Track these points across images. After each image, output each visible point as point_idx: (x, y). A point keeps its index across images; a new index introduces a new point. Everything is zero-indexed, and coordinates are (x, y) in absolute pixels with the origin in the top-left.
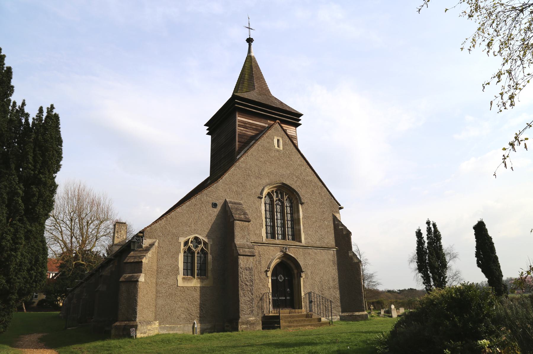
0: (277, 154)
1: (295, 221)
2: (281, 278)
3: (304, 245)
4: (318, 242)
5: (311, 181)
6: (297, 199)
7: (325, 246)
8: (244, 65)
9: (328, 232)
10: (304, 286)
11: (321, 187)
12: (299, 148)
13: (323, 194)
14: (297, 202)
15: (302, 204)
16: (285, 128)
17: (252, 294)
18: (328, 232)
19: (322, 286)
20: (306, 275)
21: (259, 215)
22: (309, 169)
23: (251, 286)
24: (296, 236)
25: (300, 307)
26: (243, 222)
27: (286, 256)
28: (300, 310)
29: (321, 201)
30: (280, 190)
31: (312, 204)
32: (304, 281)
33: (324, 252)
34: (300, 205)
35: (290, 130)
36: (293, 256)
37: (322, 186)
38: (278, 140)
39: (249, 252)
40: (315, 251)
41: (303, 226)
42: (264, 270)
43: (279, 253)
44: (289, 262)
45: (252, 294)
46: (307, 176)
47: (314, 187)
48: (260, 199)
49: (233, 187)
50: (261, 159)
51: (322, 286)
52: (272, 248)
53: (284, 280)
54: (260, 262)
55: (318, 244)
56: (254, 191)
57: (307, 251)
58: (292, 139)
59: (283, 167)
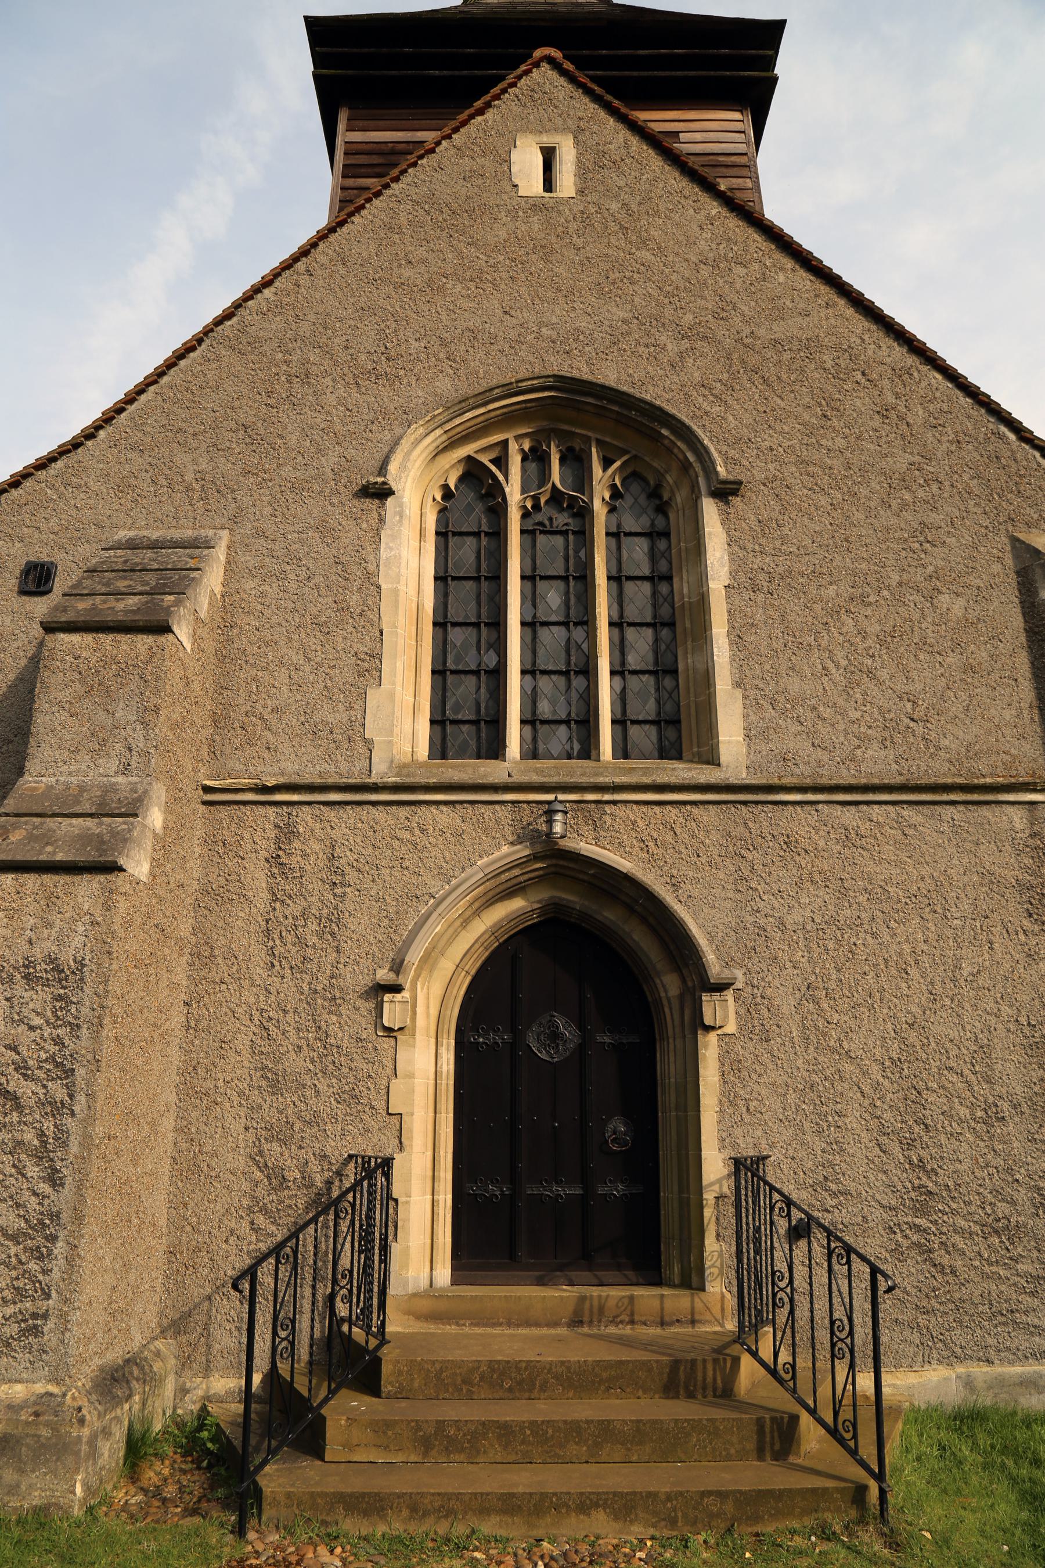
0: (536, 222)
1: (672, 626)
2: (553, 1038)
3: (743, 777)
4: (874, 751)
5: (810, 346)
6: (686, 466)
7: (942, 771)
8: (760, 193)
9: (970, 669)
10: (729, 1098)
11: (900, 374)
12: (773, 212)
13: (918, 415)
14: (694, 489)
15: (725, 492)
16: (657, 127)
17: (54, 1179)
18: (970, 669)
19: (915, 1098)
20: (749, 1009)
21: (354, 600)
22: (788, 275)
23: (56, 1108)
24: (675, 722)
25: (692, 1279)
26: (107, 640)
27: (556, 863)
28: (676, 1300)
29: (901, 461)
30: (563, 436)
31: (816, 488)
32: (731, 1066)
33: (932, 826)
34: (710, 509)
35: (707, 130)
36: (623, 864)
37: (911, 360)
38: (549, 156)
39: (85, 838)
40: (849, 816)
41: (737, 639)
42: (366, 981)
43: (505, 849)
44: (610, 915)
45: (54, 1179)
46: (779, 314)
47: (838, 375)
48: (371, 504)
49: (182, 458)
50: (407, 273)
51: (915, 1098)
52: (444, 817)
53: (581, 1048)
54: (332, 925)
55: (878, 763)
56: (330, 461)
57: (763, 820)
58: (708, 173)
59: (570, 295)
